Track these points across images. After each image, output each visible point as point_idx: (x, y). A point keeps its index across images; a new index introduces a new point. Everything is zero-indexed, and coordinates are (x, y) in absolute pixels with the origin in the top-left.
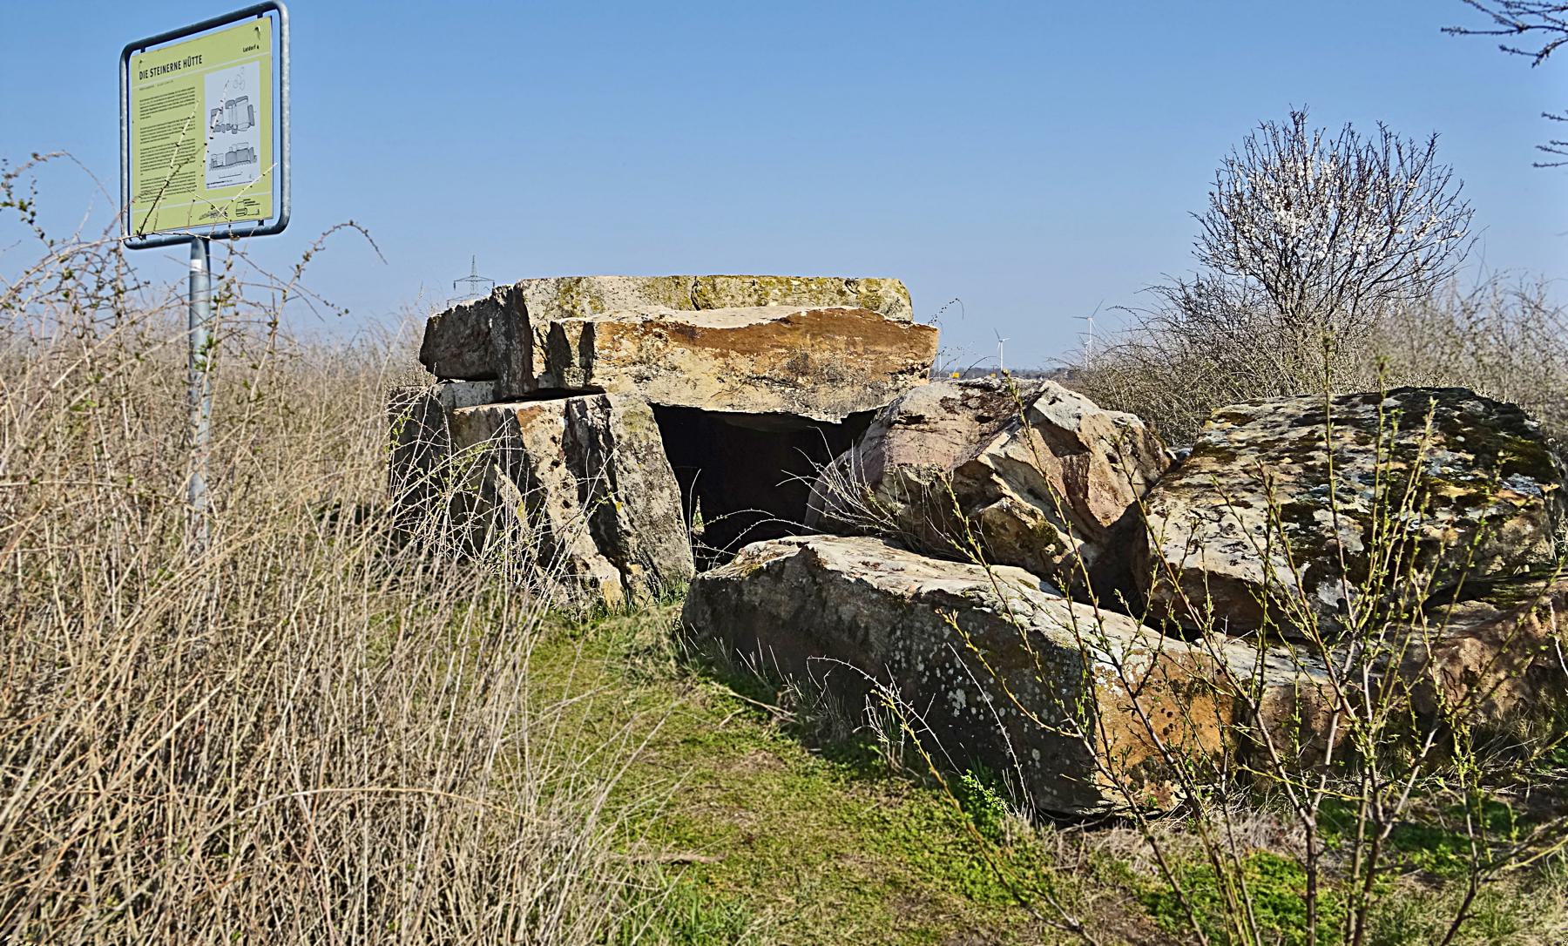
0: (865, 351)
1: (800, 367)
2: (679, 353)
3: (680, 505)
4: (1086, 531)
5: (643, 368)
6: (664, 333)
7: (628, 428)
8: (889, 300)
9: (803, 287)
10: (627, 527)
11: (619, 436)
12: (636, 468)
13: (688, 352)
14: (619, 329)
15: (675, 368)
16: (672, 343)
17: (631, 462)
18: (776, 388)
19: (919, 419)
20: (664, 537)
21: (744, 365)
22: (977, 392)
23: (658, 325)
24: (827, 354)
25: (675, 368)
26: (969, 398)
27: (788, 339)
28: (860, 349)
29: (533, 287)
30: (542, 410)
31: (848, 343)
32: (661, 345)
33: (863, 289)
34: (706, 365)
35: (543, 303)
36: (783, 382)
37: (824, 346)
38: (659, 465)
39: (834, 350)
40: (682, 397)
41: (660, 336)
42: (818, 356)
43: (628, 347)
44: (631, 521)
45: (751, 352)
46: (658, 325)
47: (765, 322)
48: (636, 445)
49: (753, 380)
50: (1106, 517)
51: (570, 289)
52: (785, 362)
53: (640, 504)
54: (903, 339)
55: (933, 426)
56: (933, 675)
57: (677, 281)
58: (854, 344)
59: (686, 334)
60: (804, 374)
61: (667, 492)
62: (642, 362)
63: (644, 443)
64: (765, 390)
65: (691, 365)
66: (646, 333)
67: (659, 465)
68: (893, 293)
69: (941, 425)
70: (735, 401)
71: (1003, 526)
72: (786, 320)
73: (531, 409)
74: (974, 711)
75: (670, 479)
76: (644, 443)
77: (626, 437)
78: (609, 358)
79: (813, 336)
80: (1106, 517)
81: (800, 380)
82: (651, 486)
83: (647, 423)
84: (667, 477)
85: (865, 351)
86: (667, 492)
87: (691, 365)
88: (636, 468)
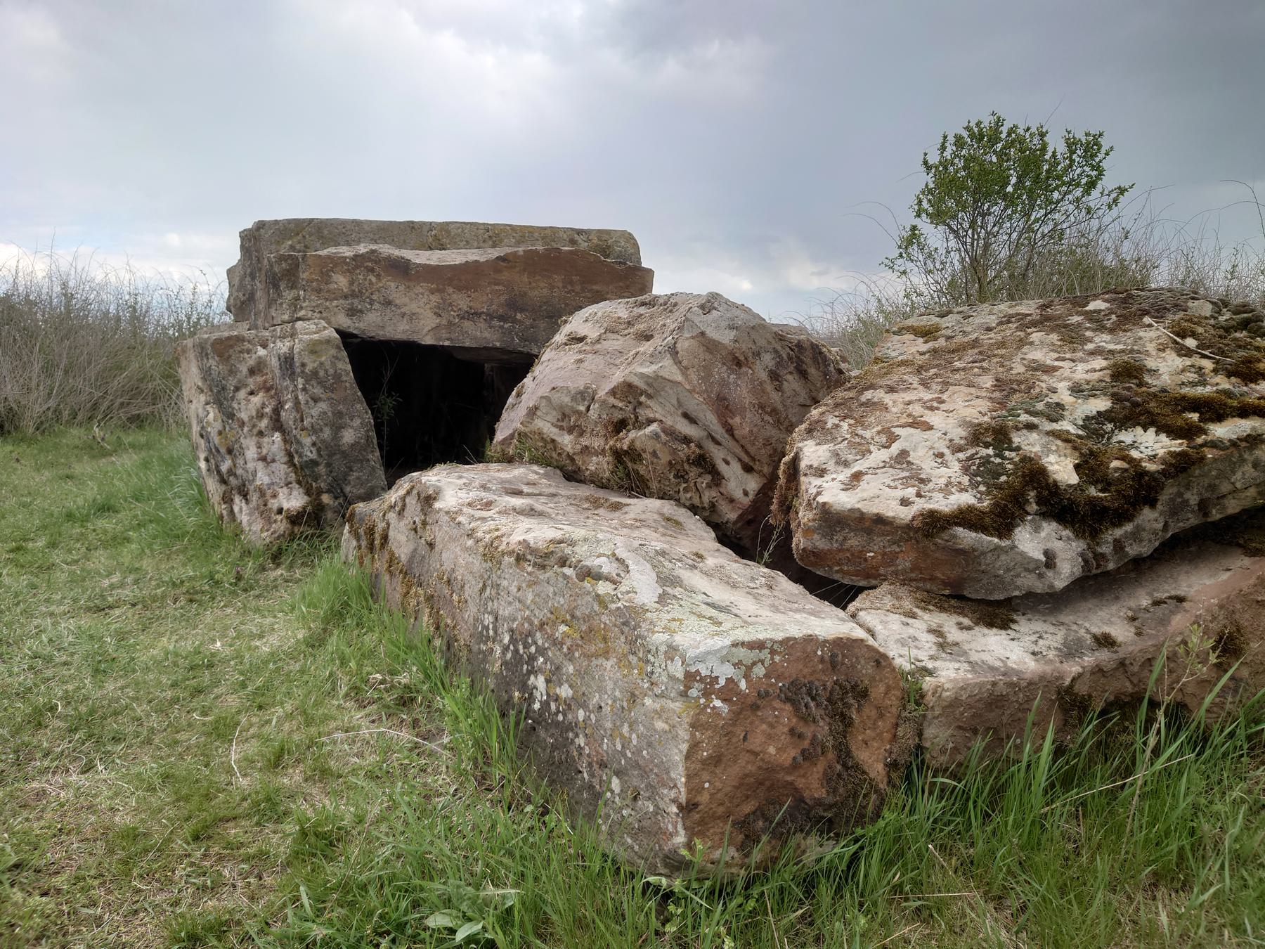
0: (583, 290)
2: (393, 288)
4: (746, 459)
5: (356, 301)
18: (496, 323)
19: (581, 340)
21: (462, 301)
27: (505, 276)
28: (578, 288)
32: (374, 279)
36: (502, 318)
39: (552, 287)
40: (398, 330)
41: (372, 270)
48: (322, 373)
49: (472, 315)
50: (746, 493)
52: (503, 299)
56: (516, 651)
58: (571, 283)
59: (401, 269)
60: (522, 310)
63: (331, 371)
64: (483, 325)
66: (357, 267)
71: (654, 454)
74: (553, 706)
75: (361, 407)
80: (746, 493)
81: (519, 316)
85: (583, 290)
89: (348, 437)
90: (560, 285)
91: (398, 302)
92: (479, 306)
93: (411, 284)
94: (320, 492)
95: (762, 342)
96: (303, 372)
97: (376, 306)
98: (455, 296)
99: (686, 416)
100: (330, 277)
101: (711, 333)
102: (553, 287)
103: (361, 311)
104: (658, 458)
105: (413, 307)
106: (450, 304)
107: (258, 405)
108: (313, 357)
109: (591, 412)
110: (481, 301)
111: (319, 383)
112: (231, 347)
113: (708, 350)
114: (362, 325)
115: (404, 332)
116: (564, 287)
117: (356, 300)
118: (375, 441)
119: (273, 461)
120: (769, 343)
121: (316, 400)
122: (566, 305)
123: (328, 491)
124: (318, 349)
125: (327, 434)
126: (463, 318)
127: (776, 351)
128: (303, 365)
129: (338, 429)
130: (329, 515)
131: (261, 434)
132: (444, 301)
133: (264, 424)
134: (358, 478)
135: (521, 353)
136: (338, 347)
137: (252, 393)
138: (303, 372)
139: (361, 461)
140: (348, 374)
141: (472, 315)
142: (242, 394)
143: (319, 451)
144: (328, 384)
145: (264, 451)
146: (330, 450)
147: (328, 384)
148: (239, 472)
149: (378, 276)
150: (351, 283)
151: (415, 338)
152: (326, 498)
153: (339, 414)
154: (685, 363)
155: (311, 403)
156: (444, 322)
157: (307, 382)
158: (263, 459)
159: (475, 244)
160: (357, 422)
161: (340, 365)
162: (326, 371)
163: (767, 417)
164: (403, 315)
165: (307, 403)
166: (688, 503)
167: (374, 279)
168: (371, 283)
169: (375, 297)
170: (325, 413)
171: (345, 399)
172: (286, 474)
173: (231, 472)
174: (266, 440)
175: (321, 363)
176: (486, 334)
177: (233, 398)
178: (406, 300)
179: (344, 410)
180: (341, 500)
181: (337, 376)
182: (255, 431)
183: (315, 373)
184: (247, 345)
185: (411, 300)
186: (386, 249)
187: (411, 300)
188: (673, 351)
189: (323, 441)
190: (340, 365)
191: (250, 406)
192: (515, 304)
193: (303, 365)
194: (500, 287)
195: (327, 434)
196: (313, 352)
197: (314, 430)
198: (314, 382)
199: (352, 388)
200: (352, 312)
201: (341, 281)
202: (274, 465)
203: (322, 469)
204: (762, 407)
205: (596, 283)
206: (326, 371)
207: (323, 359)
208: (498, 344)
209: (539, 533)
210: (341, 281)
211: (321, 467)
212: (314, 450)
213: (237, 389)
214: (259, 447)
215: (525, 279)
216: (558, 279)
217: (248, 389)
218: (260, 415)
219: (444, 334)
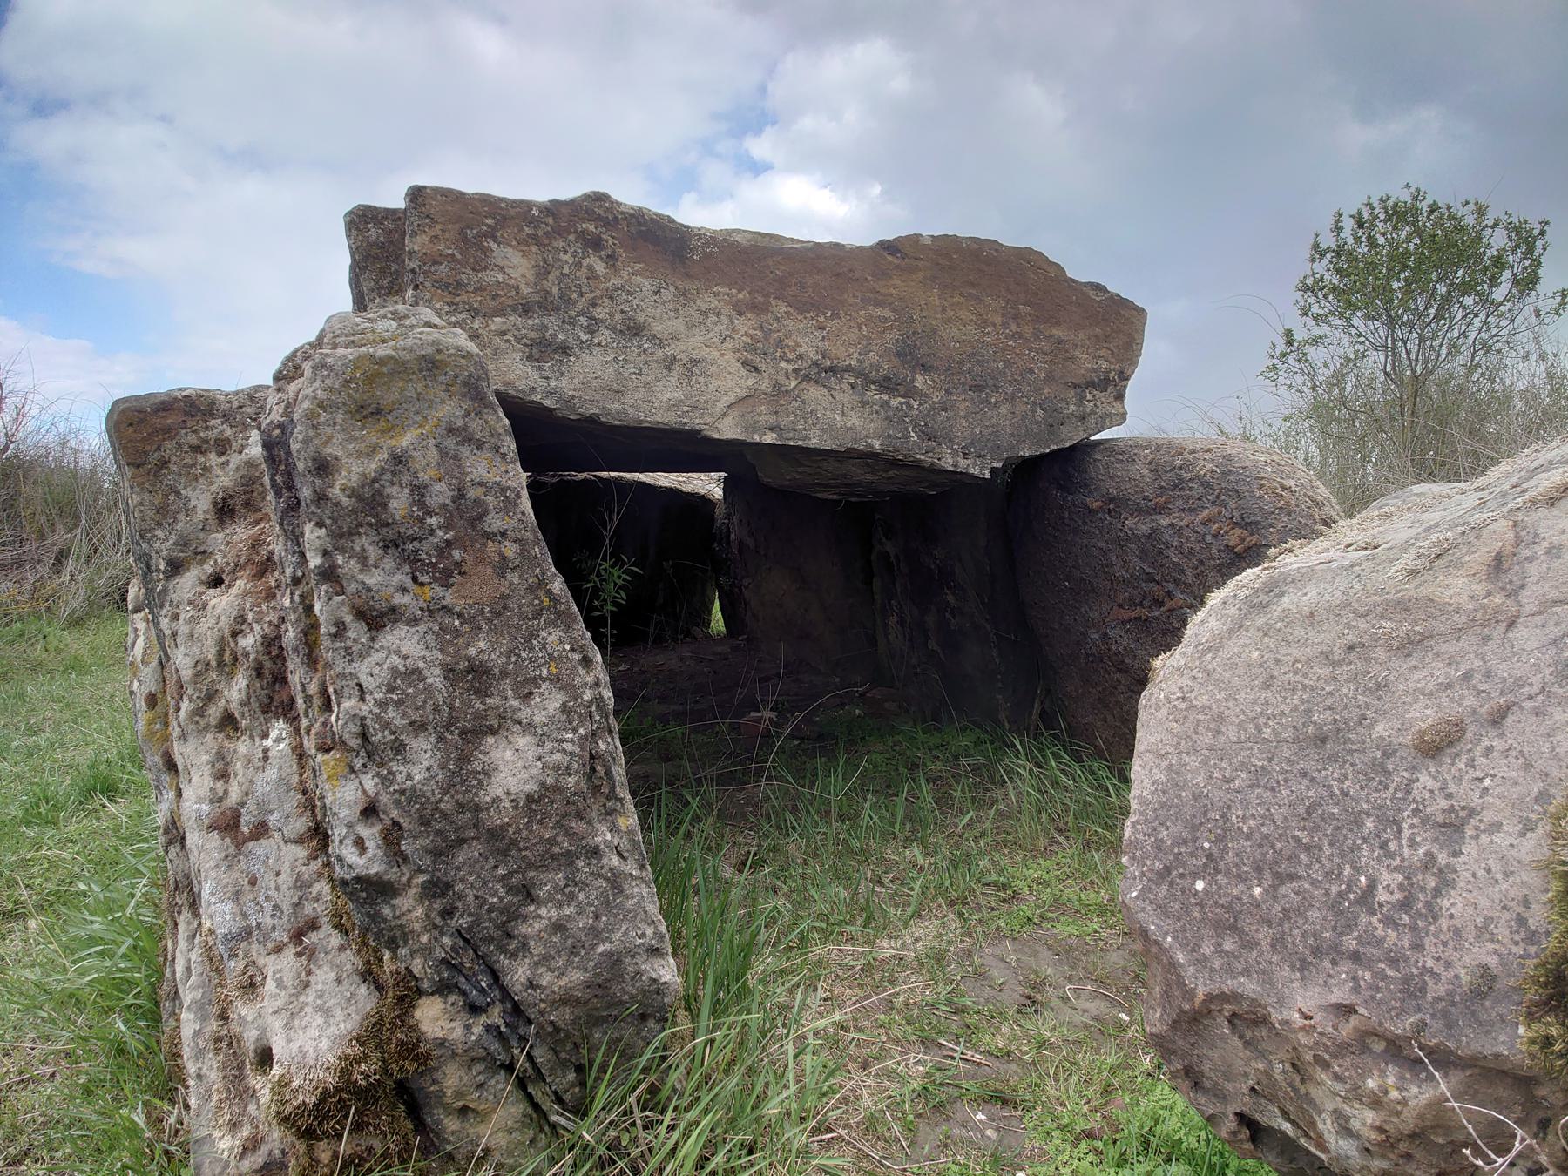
2: (648, 295)
5: (552, 321)
18: (874, 395)
28: (1028, 330)
32: (600, 268)
36: (888, 385)
41: (596, 244)
46: (592, 217)
48: (399, 503)
49: (825, 372)
52: (891, 338)
60: (926, 369)
63: (441, 493)
64: (847, 397)
66: (558, 232)
75: (565, 640)
81: (919, 381)
89: (512, 768)
90: (999, 320)
91: (657, 328)
92: (842, 352)
93: (692, 286)
94: (407, 993)
96: (320, 498)
97: (604, 336)
98: (790, 324)
100: (486, 251)
102: (985, 324)
103: (565, 350)
105: (694, 344)
106: (780, 344)
107: (225, 624)
108: (369, 434)
111: (391, 545)
112: (169, 432)
114: (565, 385)
115: (672, 405)
116: (1005, 325)
117: (550, 316)
118: (619, 772)
119: (261, 831)
121: (376, 618)
122: (1008, 364)
123: (442, 989)
124: (388, 397)
125: (422, 764)
126: (806, 378)
128: (323, 467)
129: (468, 735)
130: (452, 1078)
131: (228, 722)
132: (767, 333)
133: (236, 690)
134: (558, 927)
135: (917, 466)
137: (216, 581)
138: (320, 498)
139: (569, 858)
140: (510, 505)
141: (825, 372)
142: (187, 583)
143: (392, 835)
144: (427, 551)
146: (443, 827)
147: (427, 551)
149: (611, 259)
150: (543, 272)
151: (697, 422)
152: (434, 1018)
153: (477, 677)
155: (357, 632)
156: (765, 386)
157: (341, 536)
160: (550, 703)
161: (479, 468)
162: (419, 491)
164: (669, 364)
165: (340, 630)
167: (600, 268)
168: (593, 276)
169: (600, 313)
170: (414, 675)
171: (501, 607)
172: (301, 885)
174: (243, 747)
175: (399, 460)
176: (854, 421)
178: (678, 325)
179: (496, 659)
180: (495, 1016)
181: (467, 514)
182: (214, 712)
183: (371, 501)
184: (218, 427)
185: (690, 325)
187: (690, 325)
189: (410, 796)
190: (479, 468)
191: (206, 624)
193: (323, 467)
195: (422, 764)
196: (369, 413)
197: (370, 749)
198: (366, 542)
199: (528, 561)
201: (514, 265)
202: (260, 848)
203: (410, 908)
205: (1058, 324)
206: (419, 491)
207: (406, 440)
208: (877, 444)
210: (514, 265)
211: (404, 902)
212: (370, 833)
213: (176, 568)
215: (935, 297)
217: (209, 568)
218: (226, 661)
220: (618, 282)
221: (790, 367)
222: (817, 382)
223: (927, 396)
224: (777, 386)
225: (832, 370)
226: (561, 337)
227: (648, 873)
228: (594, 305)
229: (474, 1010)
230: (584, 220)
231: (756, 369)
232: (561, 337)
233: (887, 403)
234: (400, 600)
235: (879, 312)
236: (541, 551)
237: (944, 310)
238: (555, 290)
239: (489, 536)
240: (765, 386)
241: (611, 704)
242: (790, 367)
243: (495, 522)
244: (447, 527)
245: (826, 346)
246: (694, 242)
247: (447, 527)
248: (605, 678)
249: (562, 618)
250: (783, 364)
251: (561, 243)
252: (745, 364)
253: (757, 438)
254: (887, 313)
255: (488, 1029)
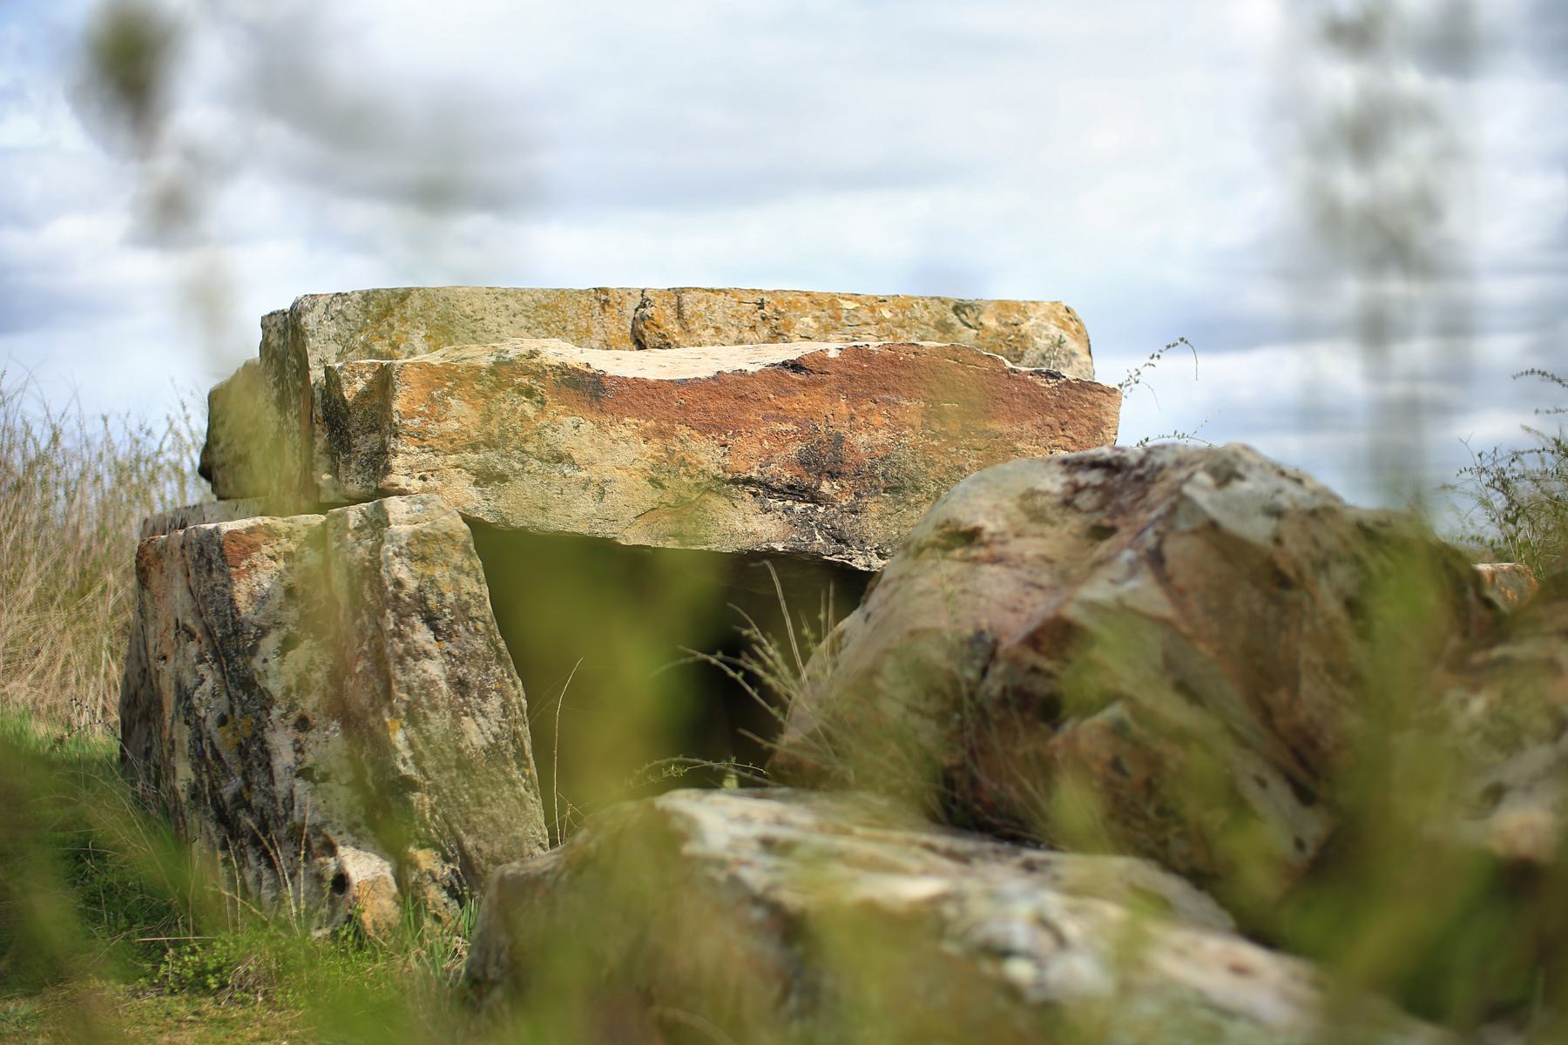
0: (965, 433)
1: (825, 460)
2: (573, 430)
3: (524, 729)
4: (1302, 776)
5: (493, 456)
6: (537, 386)
7: (419, 568)
8: (1043, 343)
9: (864, 315)
10: (408, 770)
11: (399, 584)
12: (433, 648)
13: (588, 426)
14: (445, 380)
15: (559, 459)
16: (554, 408)
17: (422, 636)
19: (971, 536)
20: (488, 794)
21: (707, 454)
22: (1095, 477)
23: (526, 372)
24: (882, 436)
25: (559, 459)
26: (1077, 489)
27: (803, 402)
28: (954, 427)
29: (320, 310)
30: (271, 533)
31: (928, 415)
33: (991, 323)
34: (626, 454)
35: (337, 338)
36: (794, 491)
37: (876, 420)
38: (480, 644)
39: (897, 428)
41: (529, 393)
42: (863, 438)
43: (461, 415)
44: (418, 760)
45: (721, 429)
46: (526, 372)
47: (751, 369)
48: (432, 601)
51: (388, 311)
52: (794, 449)
53: (438, 723)
54: (1044, 407)
55: (997, 549)
57: (603, 298)
58: (941, 416)
59: (589, 389)
60: (833, 476)
61: (495, 702)
62: (491, 444)
64: (748, 504)
65: (592, 452)
66: (499, 386)
67: (480, 644)
68: (1054, 331)
69: (1015, 547)
70: (688, 528)
72: (795, 366)
73: (251, 531)
76: (450, 597)
77: (412, 585)
78: (420, 436)
79: (854, 399)
81: (826, 487)
82: (461, 686)
83: (457, 558)
84: (496, 670)
85: (965, 433)
86: (495, 702)
87: (592, 452)
88: (433, 648)
89: (476, 734)
90: (917, 421)
92: (742, 466)
93: (606, 420)
95: (1329, 541)
98: (693, 445)
99: (1182, 687)
101: (1230, 523)
102: (902, 425)
103: (503, 478)
104: (1123, 773)
109: (989, 681)
110: (748, 454)
113: (1226, 556)
119: (325, 778)
120: (1345, 543)
126: (709, 489)
127: (1357, 560)
136: (466, 549)
140: (481, 605)
145: (310, 759)
147: (441, 625)
148: (257, 800)
150: (487, 418)
154: (1180, 581)
158: (304, 773)
159: (734, 333)
163: (1342, 692)
166: (1182, 866)
168: (525, 418)
169: (530, 447)
173: (240, 800)
177: (253, 651)
186: (559, 351)
188: (1156, 559)
191: (286, 668)
192: (825, 460)
194: (790, 426)
200: (485, 478)
204: (1331, 669)
209: (916, 888)
214: (300, 750)
215: (843, 406)
216: (912, 409)
219: (667, 522)
220: (544, 422)
221: (692, 482)
222: (718, 493)
223: (833, 500)
224: (679, 498)
225: (735, 482)
226: (500, 467)
227: (540, 801)
228: (526, 441)
229: (447, 860)
230: (518, 376)
231: (662, 487)
232: (500, 467)
233: (790, 508)
234: (428, 647)
235: (783, 427)
236: (494, 626)
237: (852, 418)
238: (496, 432)
239: (471, 619)
240: (669, 498)
241: (525, 706)
242: (692, 482)
243: (474, 612)
244: (452, 614)
245: (727, 460)
246: (607, 384)
247: (452, 614)
248: (523, 694)
249: (500, 659)
250: (685, 479)
251: (501, 395)
252: (652, 481)
253: (660, 544)
254: (790, 426)
255: (453, 871)
